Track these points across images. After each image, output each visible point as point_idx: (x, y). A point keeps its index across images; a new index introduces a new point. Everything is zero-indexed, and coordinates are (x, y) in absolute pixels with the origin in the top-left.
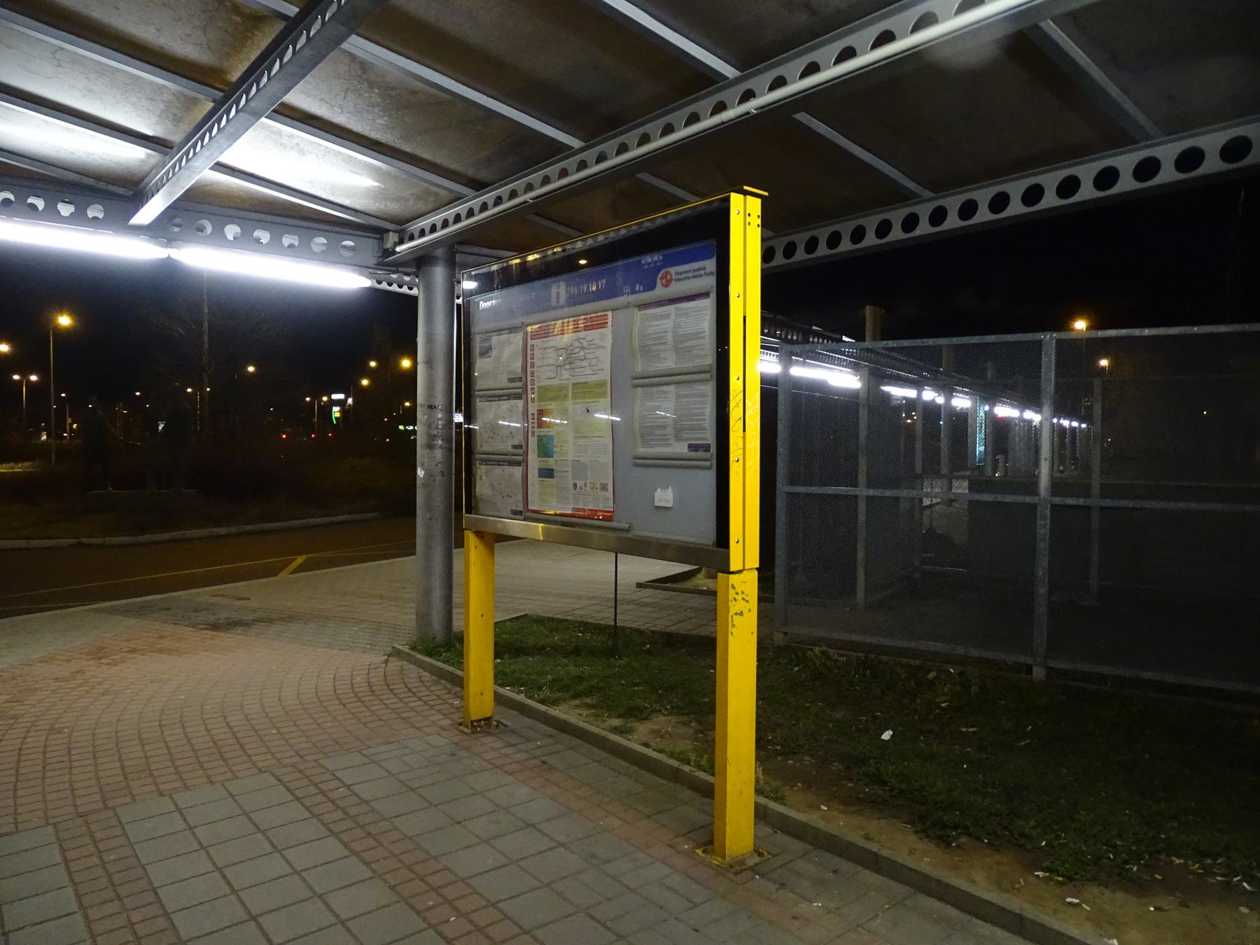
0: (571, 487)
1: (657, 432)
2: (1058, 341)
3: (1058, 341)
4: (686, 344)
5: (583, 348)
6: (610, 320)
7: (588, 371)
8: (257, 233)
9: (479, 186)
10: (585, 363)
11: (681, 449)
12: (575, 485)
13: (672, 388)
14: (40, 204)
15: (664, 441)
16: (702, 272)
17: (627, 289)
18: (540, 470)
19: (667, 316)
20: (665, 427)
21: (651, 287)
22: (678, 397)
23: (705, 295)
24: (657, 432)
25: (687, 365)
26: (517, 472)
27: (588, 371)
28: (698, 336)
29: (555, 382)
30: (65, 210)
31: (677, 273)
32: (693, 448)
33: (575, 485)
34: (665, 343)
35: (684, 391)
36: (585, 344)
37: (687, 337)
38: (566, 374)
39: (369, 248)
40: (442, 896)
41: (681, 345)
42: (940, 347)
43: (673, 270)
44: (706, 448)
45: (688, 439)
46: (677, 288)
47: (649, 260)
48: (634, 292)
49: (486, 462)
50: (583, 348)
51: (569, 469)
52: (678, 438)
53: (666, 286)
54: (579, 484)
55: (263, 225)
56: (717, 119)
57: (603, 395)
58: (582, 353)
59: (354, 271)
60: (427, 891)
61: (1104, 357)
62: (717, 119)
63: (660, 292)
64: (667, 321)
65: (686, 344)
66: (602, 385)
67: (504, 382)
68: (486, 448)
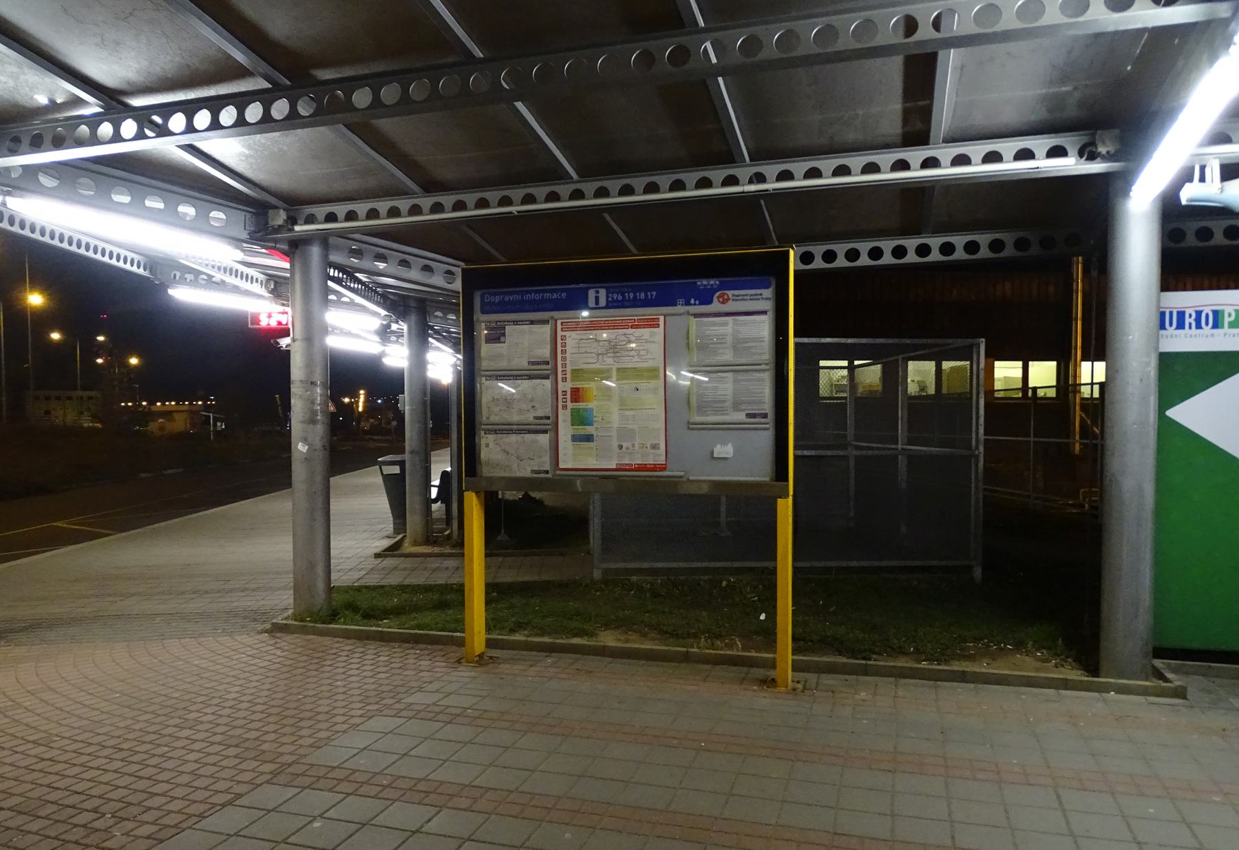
0: (616, 449)
6: (661, 323)
8: (182, 209)
9: (431, 186)
11: (741, 416)
12: (621, 447)
13: (730, 375)
14: (126, 199)
15: (721, 411)
18: (573, 436)
19: (726, 324)
20: (724, 401)
21: (710, 302)
22: (735, 381)
23: (764, 313)
26: (544, 439)
27: (636, 359)
28: (760, 340)
29: (597, 366)
30: (187, 210)
33: (621, 447)
35: (740, 377)
37: (746, 340)
38: (610, 361)
39: (240, 222)
42: (796, 344)
43: (730, 293)
44: (765, 416)
46: (731, 306)
48: (688, 304)
49: (488, 432)
51: (614, 433)
53: (723, 303)
54: (625, 445)
55: (189, 199)
56: (753, 188)
59: (230, 244)
61: (52, 341)
62: (753, 188)
63: (716, 306)
67: (525, 364)
68: (494, 419)
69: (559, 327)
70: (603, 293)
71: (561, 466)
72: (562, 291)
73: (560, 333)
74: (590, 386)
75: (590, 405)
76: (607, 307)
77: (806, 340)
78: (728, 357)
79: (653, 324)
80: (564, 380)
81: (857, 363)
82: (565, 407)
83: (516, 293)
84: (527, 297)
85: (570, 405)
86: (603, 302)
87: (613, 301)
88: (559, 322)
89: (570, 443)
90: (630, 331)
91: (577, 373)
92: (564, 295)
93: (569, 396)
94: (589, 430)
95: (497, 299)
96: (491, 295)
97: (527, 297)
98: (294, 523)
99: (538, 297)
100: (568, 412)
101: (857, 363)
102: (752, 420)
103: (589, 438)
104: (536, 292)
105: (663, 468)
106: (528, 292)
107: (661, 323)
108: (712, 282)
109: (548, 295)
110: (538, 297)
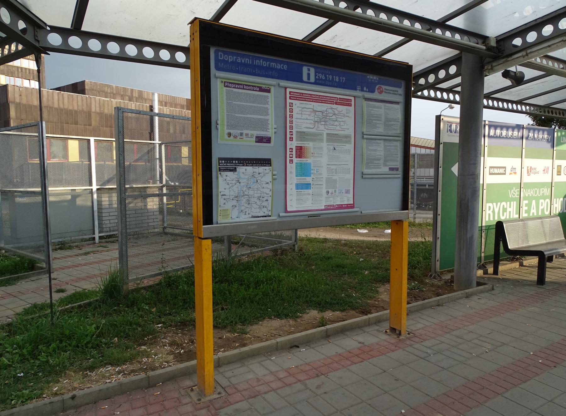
1: (375, 162)
2: (296, 157)
3: (296, 157)
4: (390, 123)
5: (334, 114)
6: (353, 103)
7: (338, 128)
10: (336, 123)
11: (386, 170)
13: (382, 142)
16: (396, 93)
17: (359, 87)
19: (381, 108)
20: (379, 160)
23: (397, 103)
24: (375, 162)
25: (390, 133)
27: (338, 128)
29: (314, 130)
31: (385, 89)
32: (391, 169)
33: (328, 192)
34: (381, 120)
36: (336, 112)
40: (284, 383)
41: (388, 123)
44: (397, 169)
45: (389, 165)
47: (371, 77)
48: (362, 90)
50: (334, 114)
52: (385, 165)
54: (330, 191)
57: (349, 142)
58: (334, 117)
60: (281, 370)
64: (380, 110)
65: (390, 123)
66: (348, 137)
69: (288, 95)
70: (312, 71)
71: (288, 210)
72: (284, 63)
73: (289, 101)
74: (309, 145)
75: (310, 160)
76: (315, 83)
77: (169, 164)
78: (381, 130)
79: (347, 103)
80: (291, 139)
81: (165, 198)
82: (291, 161)
83: (248, 57)
84: (257, 62)
85: (295, 160)
86: (312, 79)
87: (319, 79)
88: (288, 90)
89: (294, 190)
90: (335, 106)
91: (302, 135)
92: (285, 67)
93: (294, 153)
94: (309, 179)
95: (231, 59)
96: (225, 53)
97: (257, 62)
98: (127, 268)
99: (265, 64)
100: (294, 165)
101: (165, 198)
102: (391, 172)
103: (307, 186)
104: (264, 59)
105: (352, 206)
106: (259, 58)
107: (353, 103)
108: (375, 78)
109: (273, 64)
110: (265, 64)
